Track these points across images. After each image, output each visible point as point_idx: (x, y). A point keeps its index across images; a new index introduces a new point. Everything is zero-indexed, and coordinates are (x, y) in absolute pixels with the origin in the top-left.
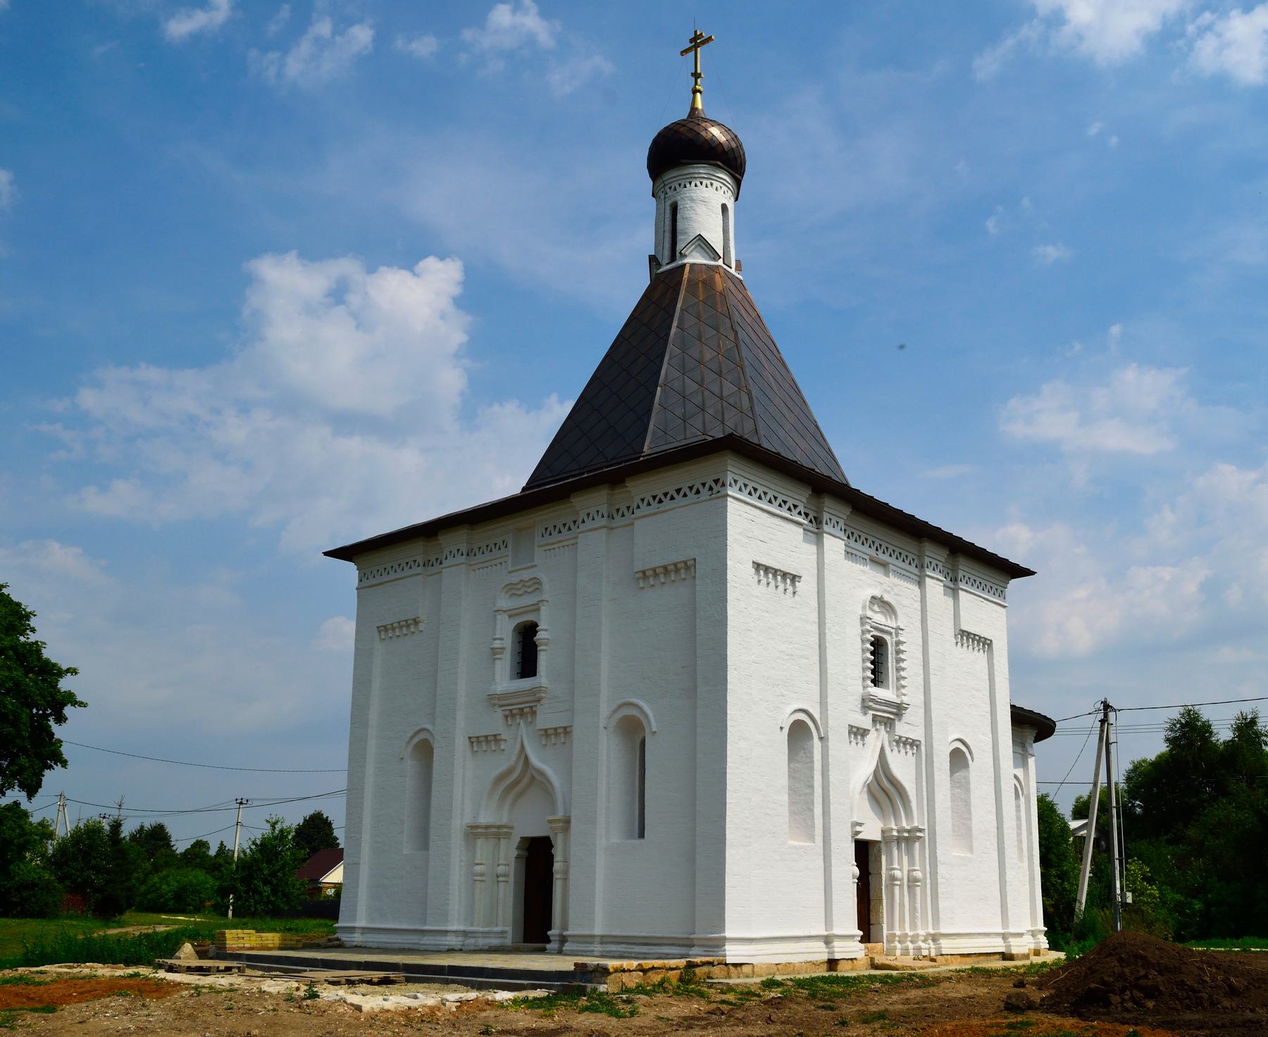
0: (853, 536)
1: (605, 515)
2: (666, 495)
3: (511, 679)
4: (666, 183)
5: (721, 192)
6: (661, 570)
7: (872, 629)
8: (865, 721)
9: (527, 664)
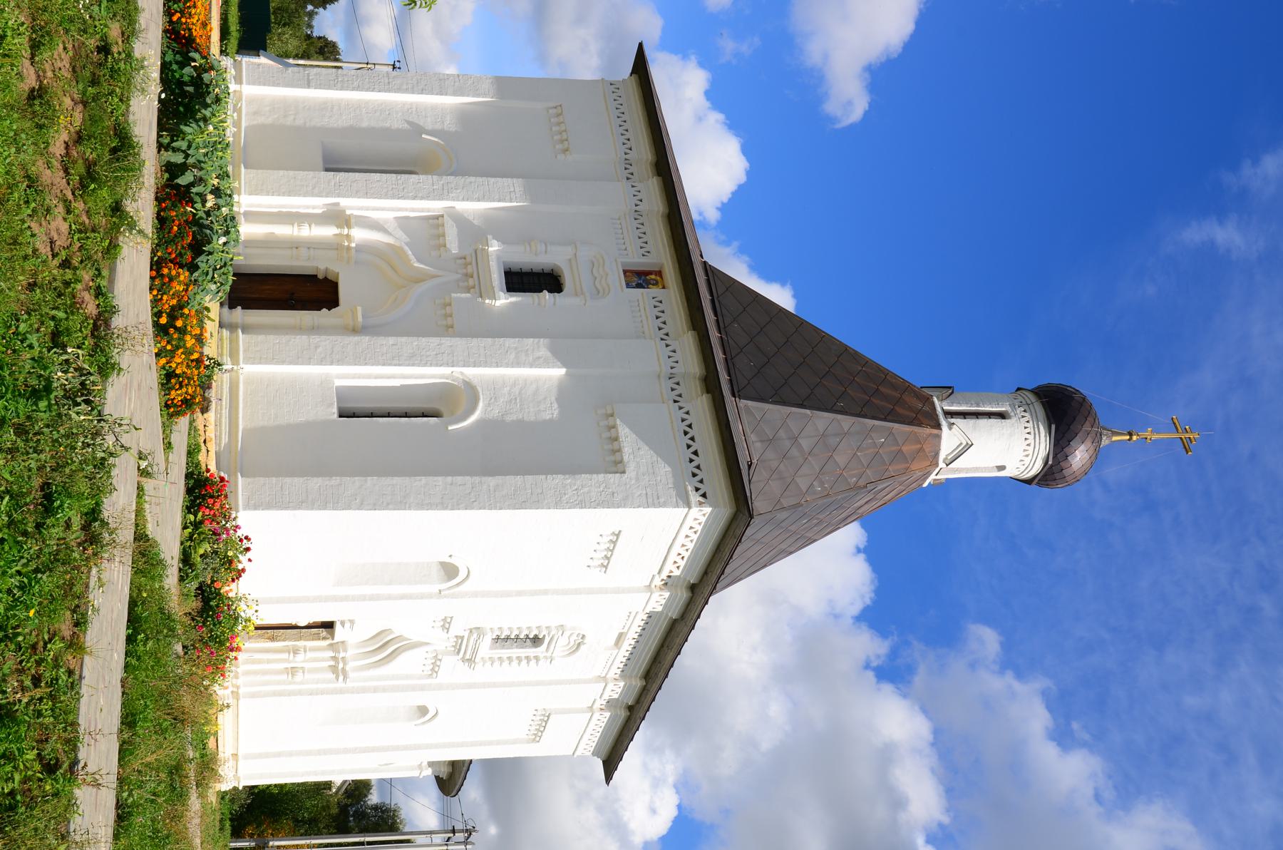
1: (673, 371)
2: (696, 453)
3: (504, 262)
4: (1031, 406)
5: (1019, 464)
6: (614, 435)
7: (551, 636)
8: (458, 629)
9: (519, 281)
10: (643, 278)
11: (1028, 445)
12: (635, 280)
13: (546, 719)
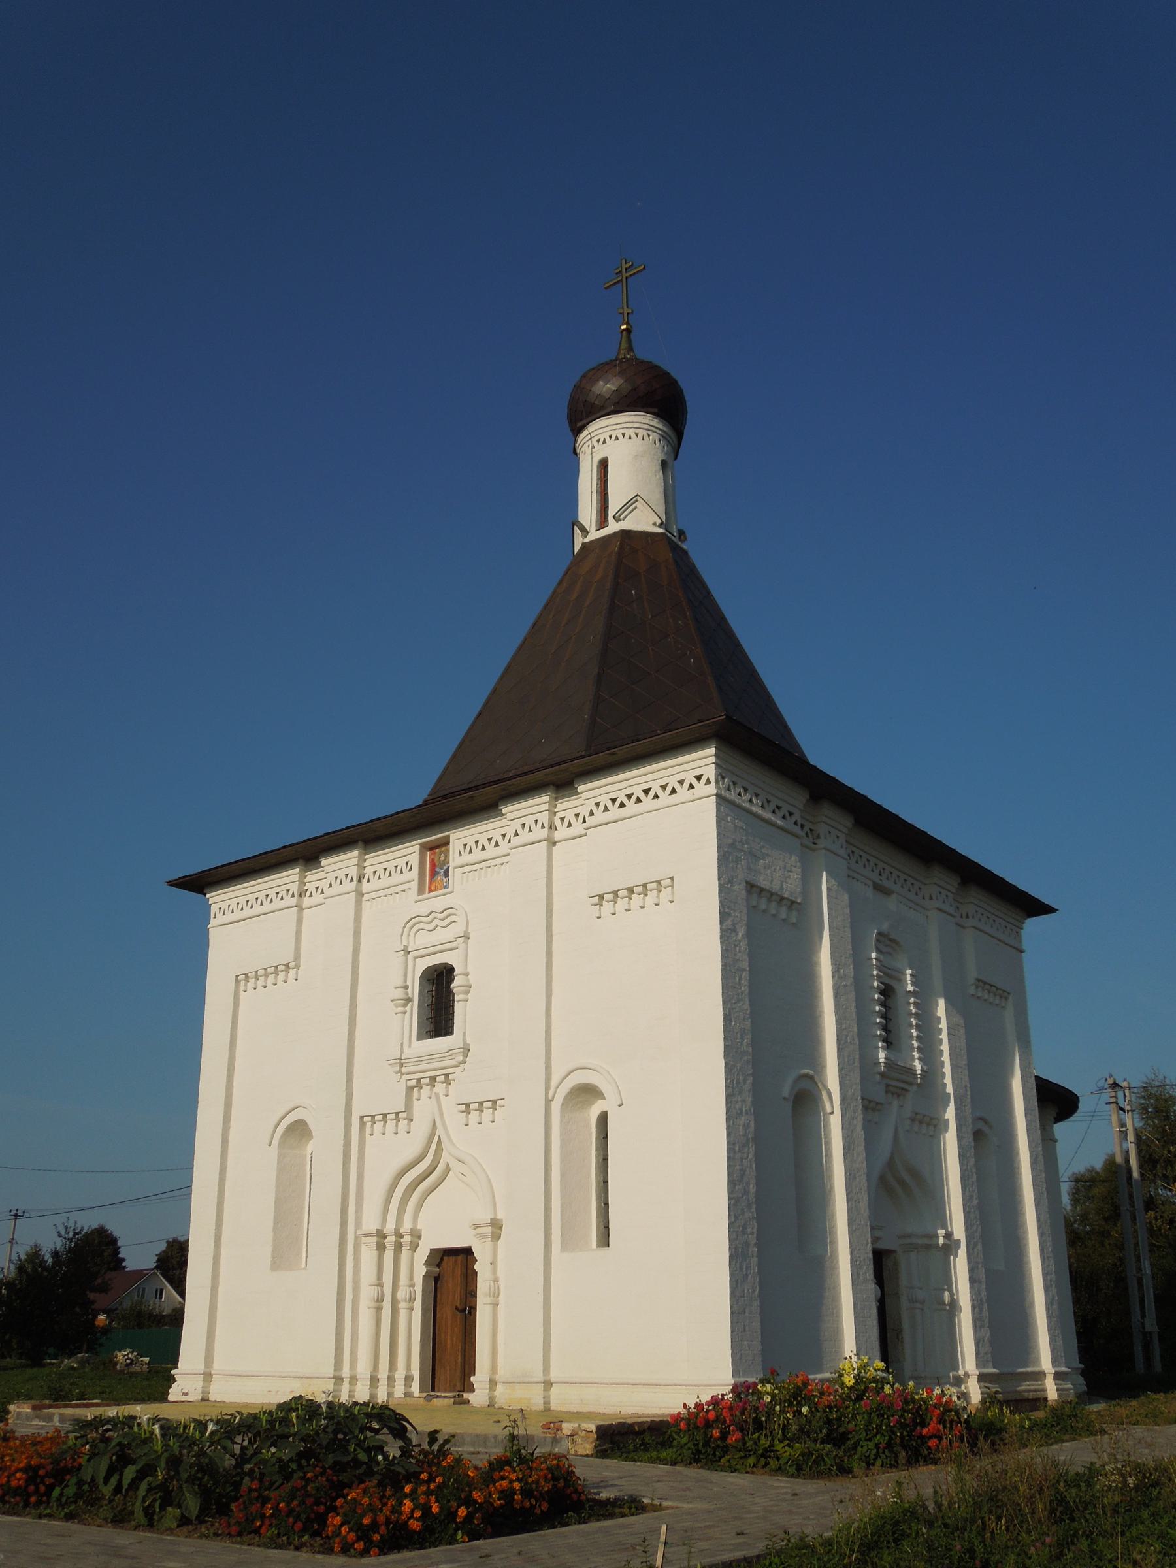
0: (853, 855)
2: (646, 792)
4: (592, 435)
10: (437, 869)
11: (637, 436)
12: (440, 878)
13: (981, 984)
